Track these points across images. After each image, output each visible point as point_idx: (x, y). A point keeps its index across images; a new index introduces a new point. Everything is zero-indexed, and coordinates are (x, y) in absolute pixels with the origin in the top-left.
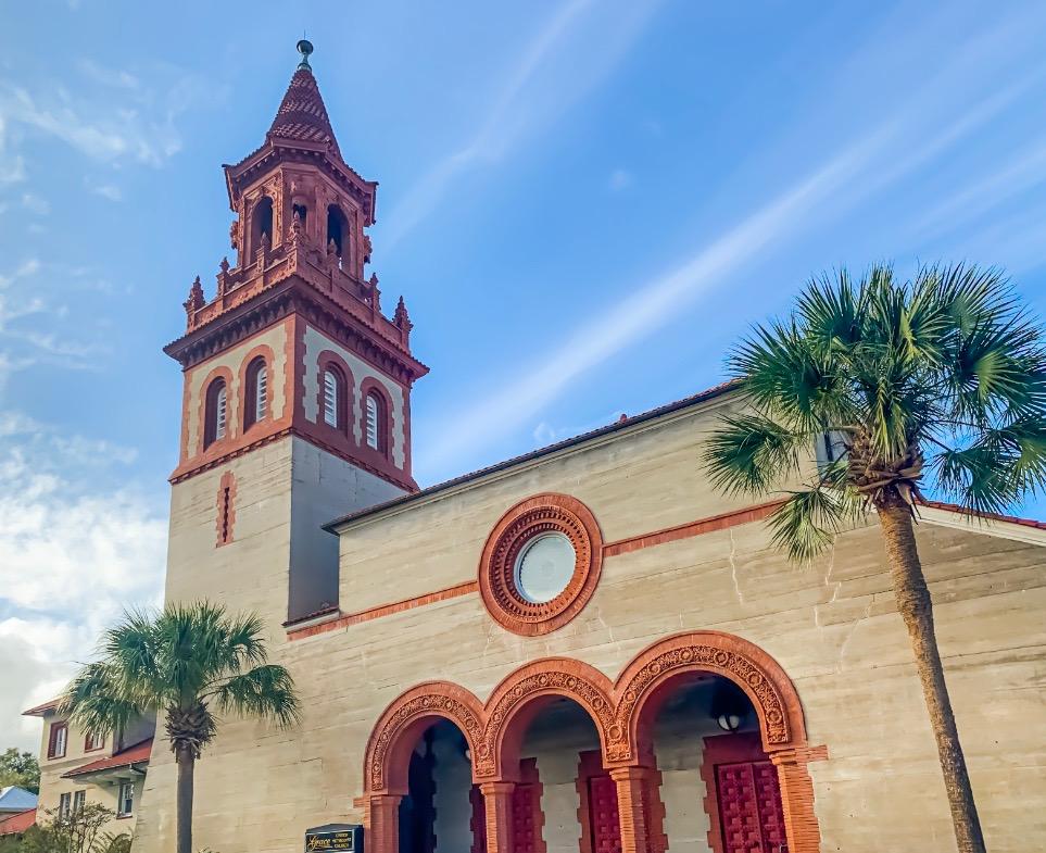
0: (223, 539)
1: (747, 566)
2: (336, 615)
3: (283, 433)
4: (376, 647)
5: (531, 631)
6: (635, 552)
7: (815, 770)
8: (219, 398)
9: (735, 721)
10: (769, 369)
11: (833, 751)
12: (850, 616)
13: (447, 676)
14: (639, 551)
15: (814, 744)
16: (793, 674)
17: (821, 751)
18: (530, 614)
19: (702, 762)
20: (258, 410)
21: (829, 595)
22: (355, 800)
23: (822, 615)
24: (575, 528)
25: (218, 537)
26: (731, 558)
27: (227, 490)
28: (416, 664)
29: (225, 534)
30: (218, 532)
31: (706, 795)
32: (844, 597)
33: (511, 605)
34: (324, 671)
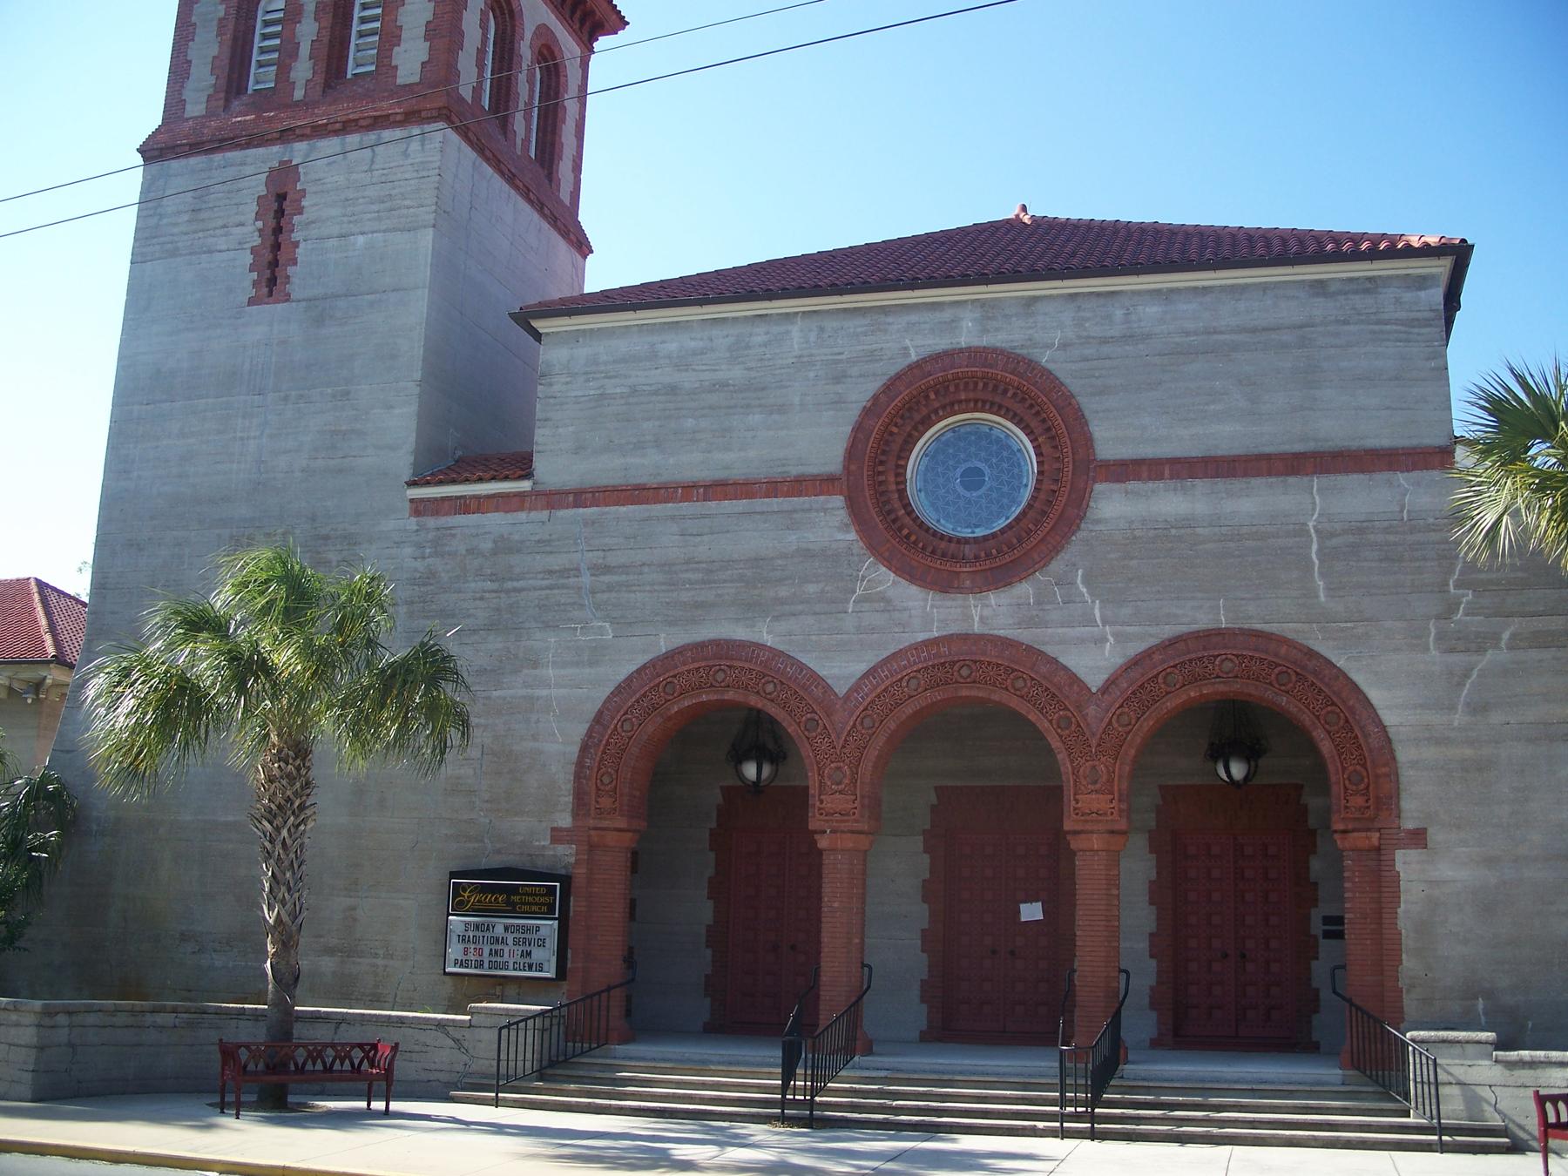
0: (266, 290)
1: (1335, 542)
2: (525, 485)
3: (423, 114)
4: (613, 559)
5: (944, 585)
6: (1150, 485)
8: (260, 13)
9: (767, 770)
10: (404, 707)
11: (1435, 835)
12: (1481, 643)
13: (765, 634)
14: (1161, 484)
15: (1409, 824)
16: (1388, 718)
17: (1418, 838)
18: (944, 555)
19: (1153, 824)
20: (356, 27)
21: (1452, 608)
22: (553, 829)
23: (1440, 637)
24: (1044, 421)
25: (255, 284)
26: (1311, 524)
27: (282, 197)
28: (698, 605)
29: (272, 282)
30: (255, 275)
31: (1153, 876)
32: (1473, 614)
33: (905, 532)
34: (495, 586)
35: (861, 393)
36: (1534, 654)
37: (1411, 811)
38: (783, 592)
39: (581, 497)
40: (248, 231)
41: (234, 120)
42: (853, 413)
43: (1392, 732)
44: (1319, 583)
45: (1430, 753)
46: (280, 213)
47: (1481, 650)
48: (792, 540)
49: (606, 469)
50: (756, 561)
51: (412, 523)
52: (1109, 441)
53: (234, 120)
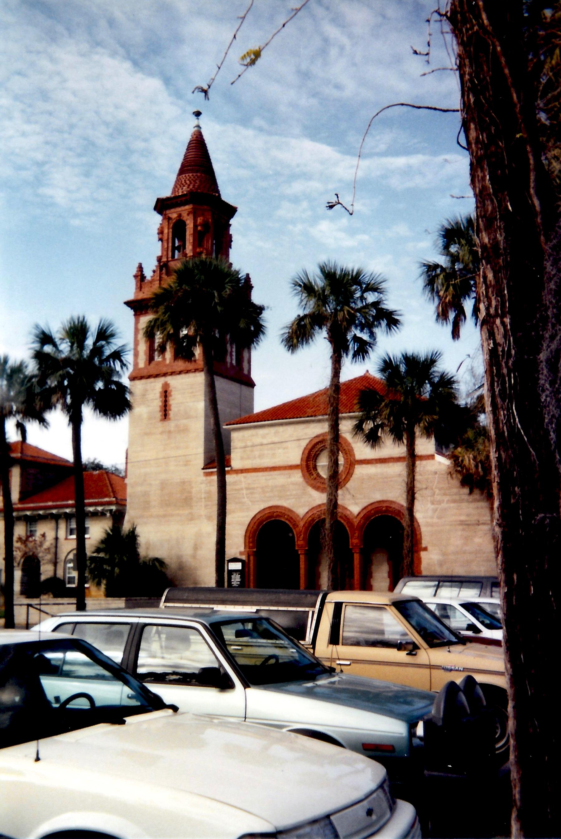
7: (423, 554)
11: (429, 548)
12: (440, 502)
35: (304, 444)
36: (452, 505)
37: (424, 544)
38: (288, 493)
39: (242, 471)
40: (158, 403)
41: (505, 281)
42: (302, 448)
43: (420, 524)
44: (12, 651)
45: (429, 529)
46: (166, 396)
47: (440, 504)
48: (289, 480)
49: (248, 464)
50: (283, 486)
51: (204, 478)
52: (297, 477)
53: (505, 281)
